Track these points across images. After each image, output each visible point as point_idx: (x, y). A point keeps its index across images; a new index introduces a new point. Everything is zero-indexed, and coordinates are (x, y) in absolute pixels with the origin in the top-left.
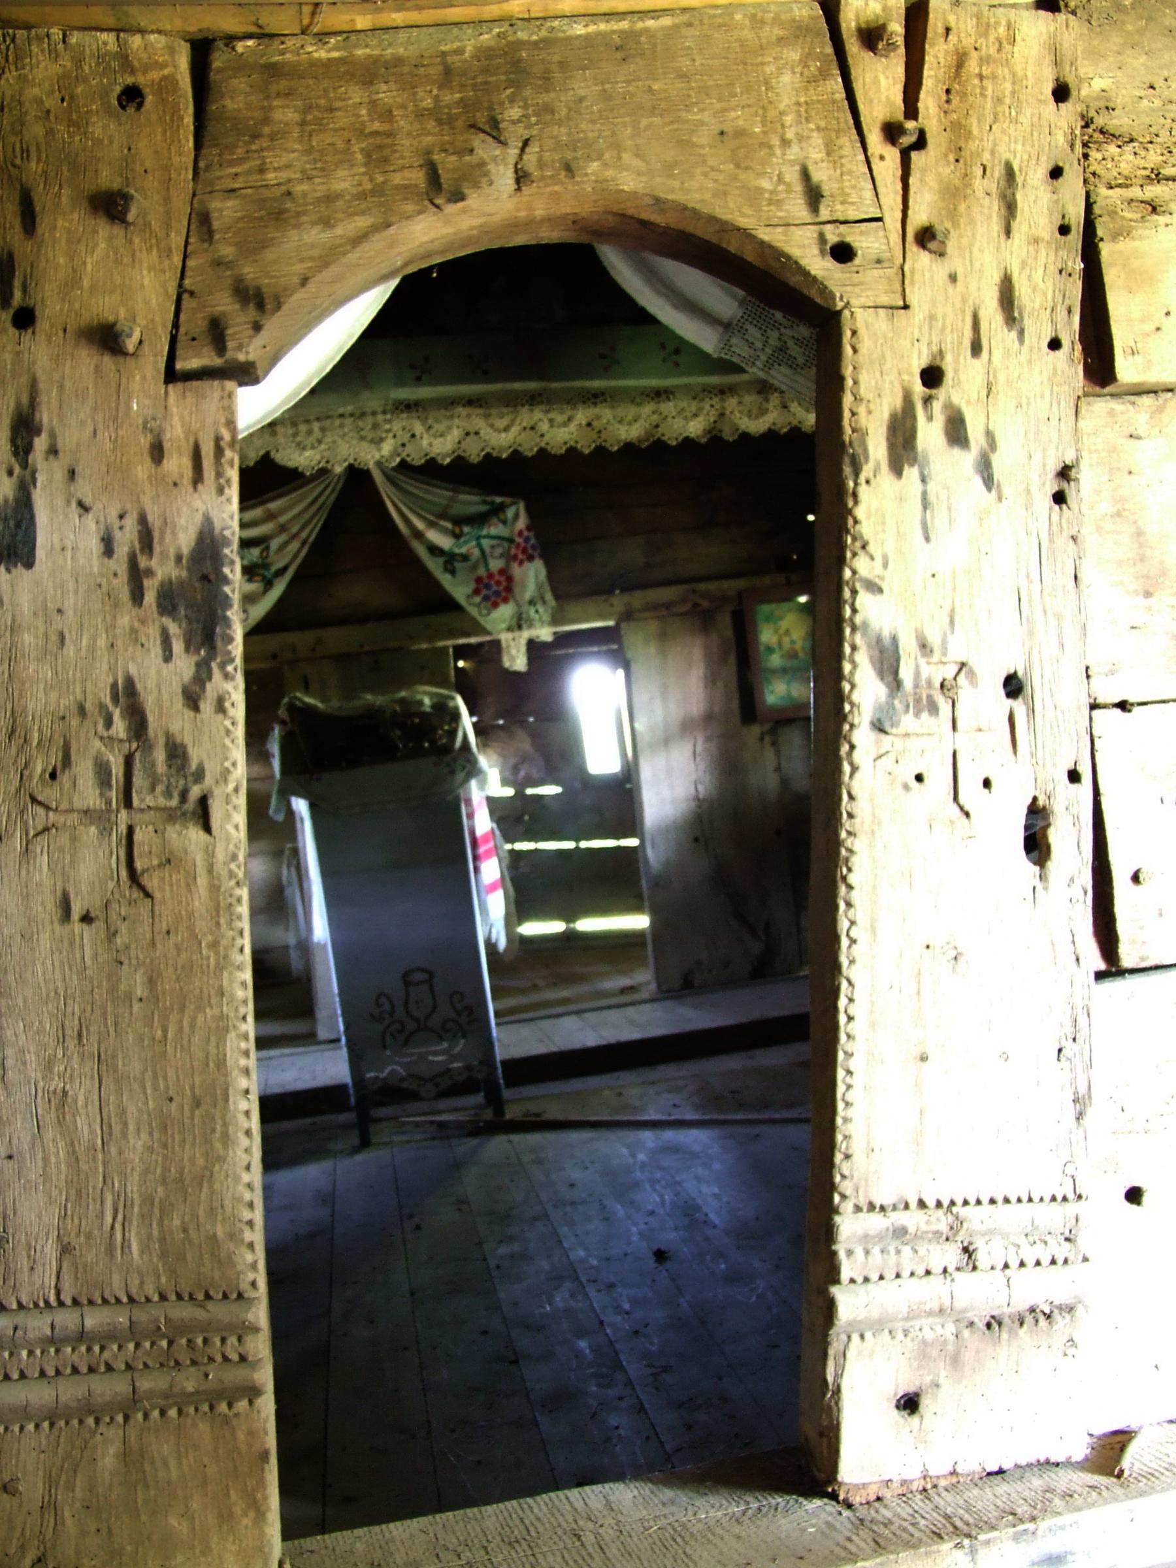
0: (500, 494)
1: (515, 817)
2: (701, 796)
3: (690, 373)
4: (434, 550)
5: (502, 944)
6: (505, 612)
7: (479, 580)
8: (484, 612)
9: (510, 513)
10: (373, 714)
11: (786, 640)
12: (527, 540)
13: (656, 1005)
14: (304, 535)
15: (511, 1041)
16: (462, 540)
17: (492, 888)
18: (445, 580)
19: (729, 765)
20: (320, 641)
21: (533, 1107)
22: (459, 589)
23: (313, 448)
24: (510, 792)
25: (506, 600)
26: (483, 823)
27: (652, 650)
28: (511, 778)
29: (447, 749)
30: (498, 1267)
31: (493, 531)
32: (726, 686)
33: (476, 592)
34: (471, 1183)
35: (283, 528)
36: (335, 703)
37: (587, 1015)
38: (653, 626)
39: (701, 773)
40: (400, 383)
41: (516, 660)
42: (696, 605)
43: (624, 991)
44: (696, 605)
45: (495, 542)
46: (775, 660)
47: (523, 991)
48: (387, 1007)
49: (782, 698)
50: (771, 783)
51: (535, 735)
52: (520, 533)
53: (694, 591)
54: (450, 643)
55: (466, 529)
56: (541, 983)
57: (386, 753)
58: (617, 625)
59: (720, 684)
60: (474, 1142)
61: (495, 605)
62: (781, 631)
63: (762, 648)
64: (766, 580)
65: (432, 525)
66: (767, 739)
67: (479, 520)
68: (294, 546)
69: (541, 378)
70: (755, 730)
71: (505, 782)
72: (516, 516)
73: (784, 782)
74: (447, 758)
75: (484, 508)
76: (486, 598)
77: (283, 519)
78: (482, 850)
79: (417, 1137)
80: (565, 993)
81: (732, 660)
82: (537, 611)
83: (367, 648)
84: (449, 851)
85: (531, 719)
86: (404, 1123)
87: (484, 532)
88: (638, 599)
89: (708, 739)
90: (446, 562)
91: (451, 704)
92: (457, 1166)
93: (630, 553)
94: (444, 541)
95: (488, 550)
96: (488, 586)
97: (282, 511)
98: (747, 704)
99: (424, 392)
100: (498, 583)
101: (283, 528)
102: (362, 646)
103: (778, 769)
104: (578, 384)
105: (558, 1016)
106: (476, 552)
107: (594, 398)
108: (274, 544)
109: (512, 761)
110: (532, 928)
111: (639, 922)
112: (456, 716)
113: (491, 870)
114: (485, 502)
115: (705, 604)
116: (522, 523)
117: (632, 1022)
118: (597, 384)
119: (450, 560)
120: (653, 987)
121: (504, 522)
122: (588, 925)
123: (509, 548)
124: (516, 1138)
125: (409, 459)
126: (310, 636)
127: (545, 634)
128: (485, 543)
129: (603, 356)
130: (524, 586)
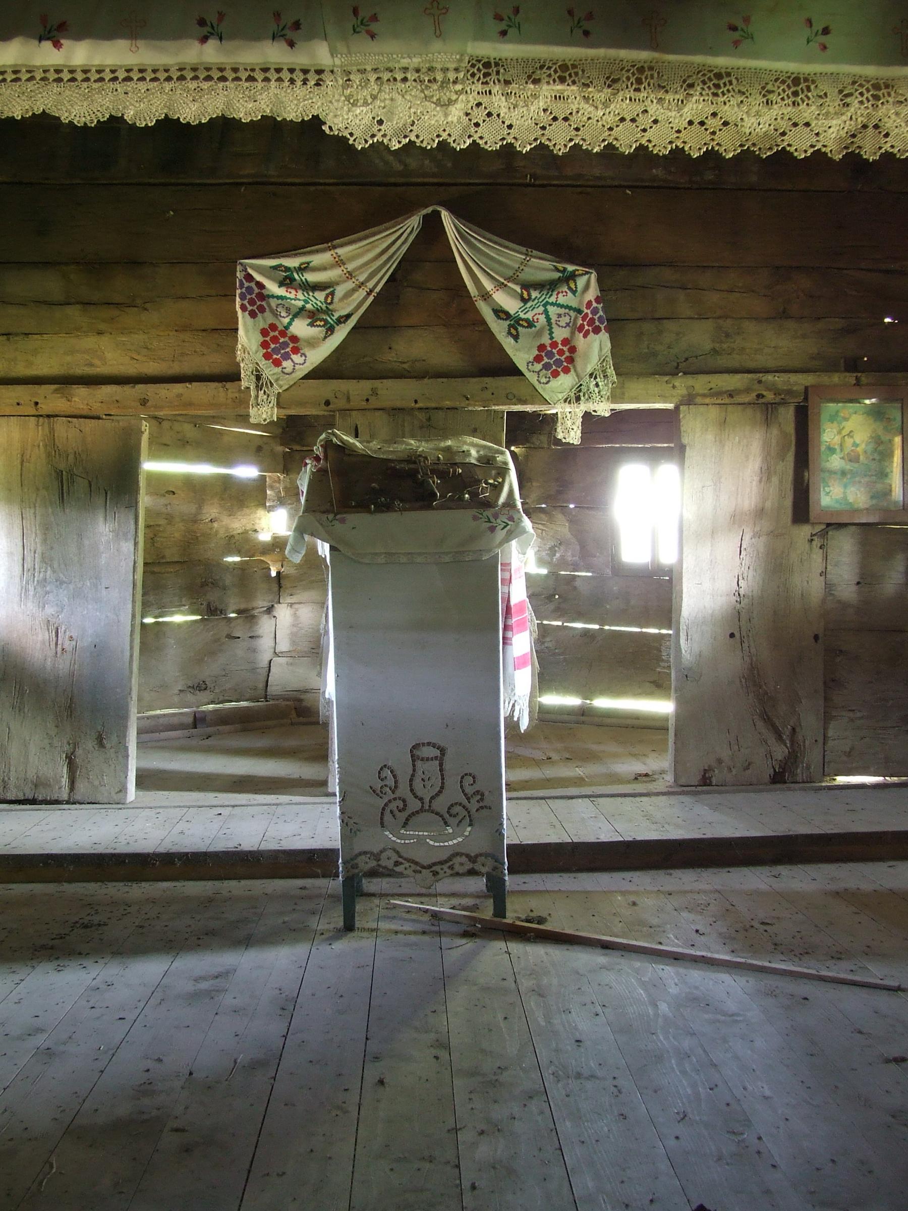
0: (572, 262)
1: (551, 595)
2: (742, 592)
3: (834, 61)
4: (500, 313)
5: (524, 725)
6: (565, 382)
7: (542, 347)
8: (544, 380)
9: (581, 282)
10: (413, 459)
11: (849, 442)
12: (595, 311)
13: (673, 800)
14: (370, 285)
15: (524, 822)
16: (529, 305)
17: (520, 663)
18: (508, 343)
19: (776, 565)
20: (374, 392)
21: (538, 906)
22: (521, 354)
23: (366, 104)
24: (544, 571)
25: (566, 371)
26: (518, 593)
27: (710, 437)
28: (547, 558)
29: (488, 504)
30: (473, 1187)
31: (562, 300)
32: (781, 482)
33: (538, 359)
34: (456, 1013)
35: (350, 275)
36: (375, 445)
37: (601, 800)
38: (714, 412)
39: (744, 569)
40: (481, 35)
41: (571, 432)
42: (759, 396)
43: (637, 778)
44: (759, 396)
45: (562, 311)
46: (835, 462)
47: (537, 763)
48: (391, 782)
49: (837, 501)
50: (816, 587)
51: (573, 521)
52: (589, 304)
53: (760, 382)
54: (506, 408)
55: (534, 294)
56: (555, 757)
57: (423, 499)
58: (677, 408)
59: (775, 480)
60: (468, 945)
61: (555, 374)
62: (844, 432)
63: (823, 448)
64: (836, 378)
65: (501, 286)
66: (817, 542)
67: (550, 286)
68: (362, 293)
69: (655, 46)
70: (805, 531)
71: (541, 562)
72: (587, 287)
73: (829, 587)
74: (489, 513)
75: (557, 275)
76: (546, 367)
77: (350, 267)
78: (514, 620)
79: (407, 927)
80: (579, 772)
81: (790, 457)
82: (597, 385)
83: (420, 405)
84: (476, 613)
85: (572, 506)
86: (395, 906)
87: (553, 299)
88: (701, 383)
89: (757, 535)
90: (510, 326)
91: (500, 458)
92: (444, 981)
93: (698, 336)
94: (511, 305)
95: (554, 318)
96: (550, 355)
97: (353, 258)
98: (801, 506)
99: (508, 50)
100: (561, 352)
101: (350, 275)
102: (416, 402)
103: (823, 573)
104: (698, 59)
105: (572, 798)
106: (542, 318)
107: (718, 82)
108: (340, 291)
109: (550, 543)
110: (552, 700)
111: (662, 707)
112: (503, 471)
113: (521, 643)
114: (557, 269)
115: (770, 396)
116: (592, 294)
117: (648, 817)
118: (722, 62)
119: (515, 325)
120: (670, 778)
121: (574, 292)
122: (603, 703)
123: (576, 318)
124: (516, 947)
125: (481, 142)
126: (365, 386)
127: (603, 409)
128: (552, 310)
129: (734, 28)
130: (586, 357)
